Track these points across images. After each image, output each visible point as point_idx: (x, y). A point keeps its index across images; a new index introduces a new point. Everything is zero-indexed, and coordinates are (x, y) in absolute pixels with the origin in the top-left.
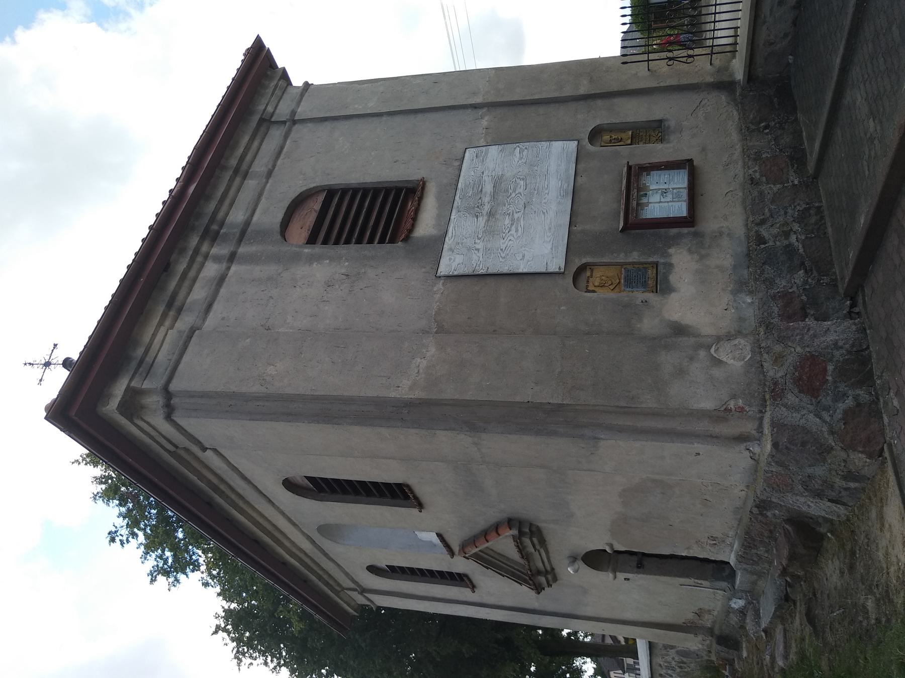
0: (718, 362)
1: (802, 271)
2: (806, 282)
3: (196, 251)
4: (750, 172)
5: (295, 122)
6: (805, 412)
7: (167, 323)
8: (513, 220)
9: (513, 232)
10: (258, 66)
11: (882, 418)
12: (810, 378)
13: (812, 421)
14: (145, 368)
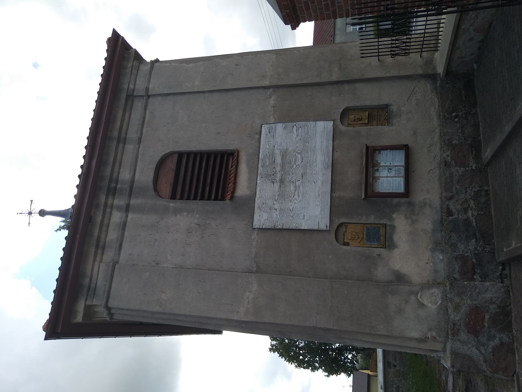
0: (422, 305)
1: (473, 241)
2: (476, 249)
3: (106, 205)
4: (445, 155)
5: (149, 96)
6: (470, 346)
7: (98, 259)
8: (295, 187)
9: (296, 197)
10: (119, 52)
11: (515, 354)
12: (474, 323)
13: (474, 352)
14: (92, 291)
